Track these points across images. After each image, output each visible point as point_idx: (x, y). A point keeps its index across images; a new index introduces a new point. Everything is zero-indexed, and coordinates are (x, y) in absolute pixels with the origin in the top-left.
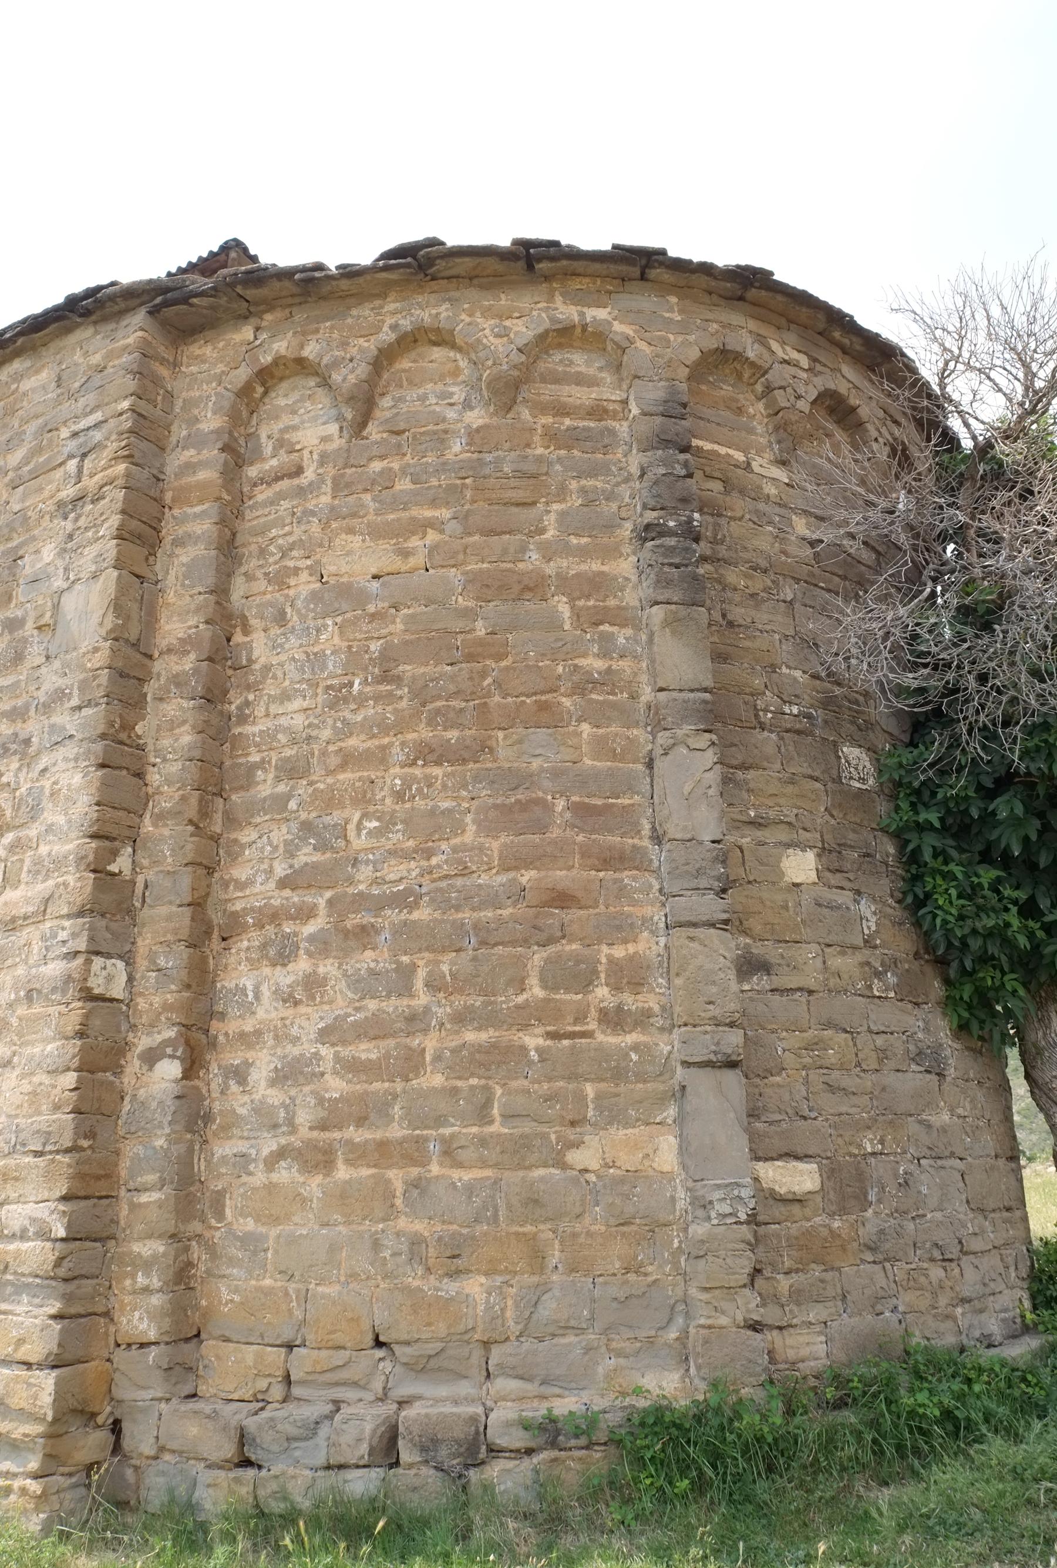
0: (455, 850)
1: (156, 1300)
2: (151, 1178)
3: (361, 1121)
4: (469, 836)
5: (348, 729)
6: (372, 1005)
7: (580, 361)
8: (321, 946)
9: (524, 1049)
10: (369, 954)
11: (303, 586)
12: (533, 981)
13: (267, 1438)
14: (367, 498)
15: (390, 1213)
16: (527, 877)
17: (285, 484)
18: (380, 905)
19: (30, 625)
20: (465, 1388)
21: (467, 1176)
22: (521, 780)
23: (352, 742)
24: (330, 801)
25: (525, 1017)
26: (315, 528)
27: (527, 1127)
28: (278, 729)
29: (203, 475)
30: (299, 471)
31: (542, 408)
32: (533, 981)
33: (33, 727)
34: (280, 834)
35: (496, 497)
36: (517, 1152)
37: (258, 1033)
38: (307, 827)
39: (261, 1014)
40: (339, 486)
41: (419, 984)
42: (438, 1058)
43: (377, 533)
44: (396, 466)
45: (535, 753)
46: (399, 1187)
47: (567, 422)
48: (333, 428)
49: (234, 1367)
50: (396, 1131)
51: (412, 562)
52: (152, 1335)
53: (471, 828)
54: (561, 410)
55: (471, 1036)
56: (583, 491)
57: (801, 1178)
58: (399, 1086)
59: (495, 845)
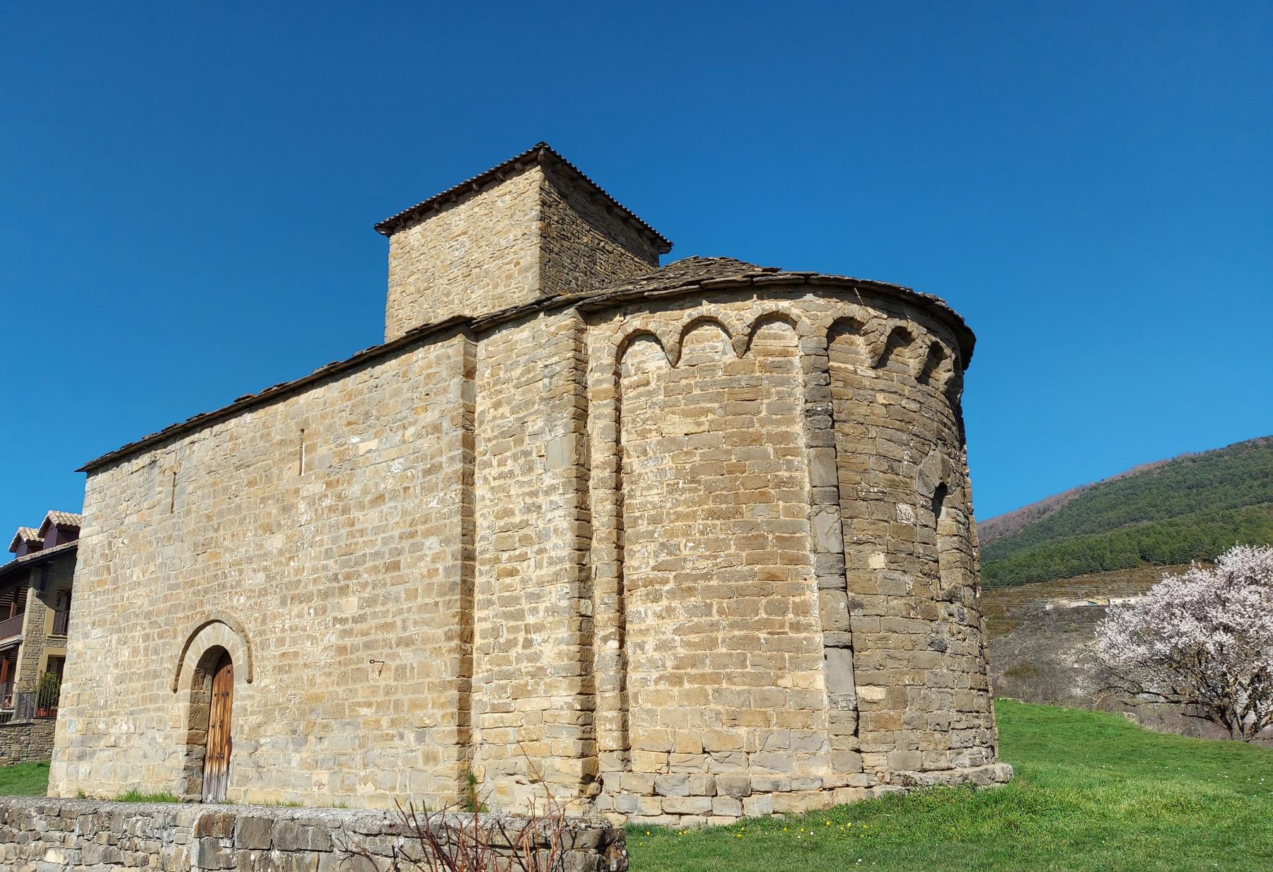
0: (727, 556)
1: (615, 734)
2: (610, 687)
3: (693, 666)
4: (732, 550)
5: (677, 503)
6: (696, 619)
7: (777, 327)
8: (672, 594)
9: (759, 639)
10: (693, 599)
11: (654, 438)
12: (762, 611)
13: (664, 785)
14: (680, 397)
15: (707, 702)
16: (757, 568)
17: (641, 389)
18: (696, 578)
19: (534, 454)
20: (739, 769)
21: (738, 688)
22: (753, 526)
23: (680, 509)
24: (672, 534)
25: (760, 625)
26: (658, 411)
27: (761, 670)
28: (647, 502)
29: (605, 386)
30: (648, 383)
31: (759, 353)
32: (762, 611)
33: (541, 499)
34: (652, 547)
35: (741, 397)
36: (757, 679)
37: (647, 630)
38: (662, 545)
39: (648, 622)
40: (668, 392)
41: (714, 611)
42: (723, 641)
43: (685, 414)
44: (692, 382)
45: (758, 514)
46: (710, 692)
47: (770, 359)
48: (663, 363)
49: (642, 761)
50: (708, 670)
51: (702, 428)
52: (615, 747)
53: (733, 547)
54: (768, 354)
55: (736, 633)
56: (778, 393)
57: (877, 693)
58: (708, 652)
59: (744, 554)
